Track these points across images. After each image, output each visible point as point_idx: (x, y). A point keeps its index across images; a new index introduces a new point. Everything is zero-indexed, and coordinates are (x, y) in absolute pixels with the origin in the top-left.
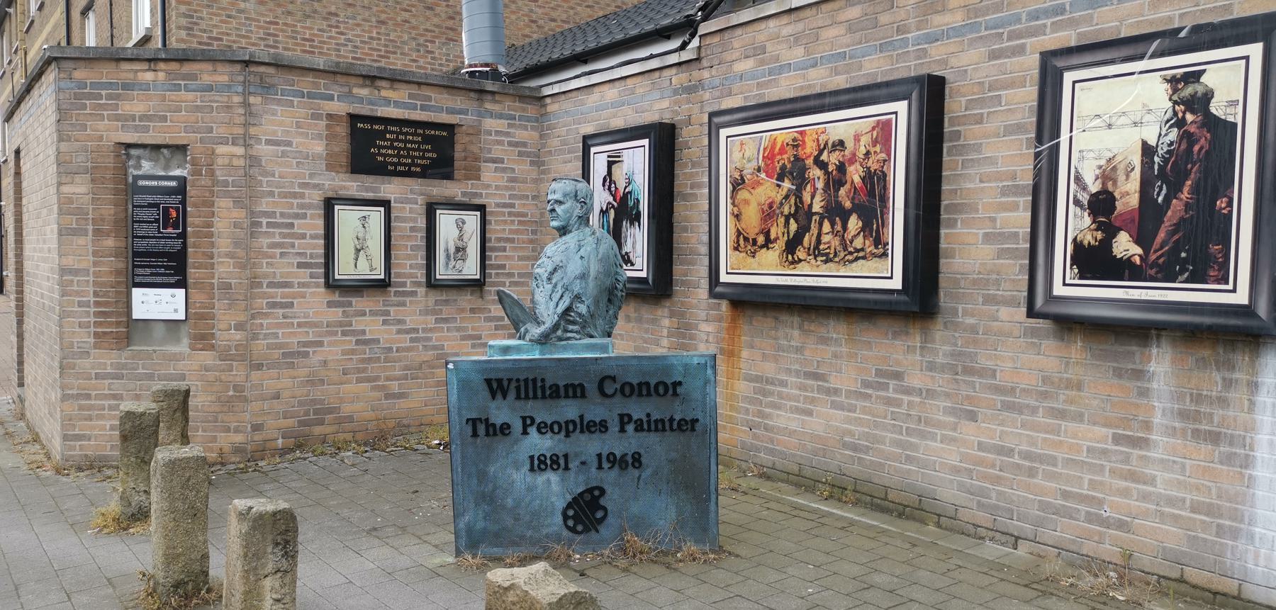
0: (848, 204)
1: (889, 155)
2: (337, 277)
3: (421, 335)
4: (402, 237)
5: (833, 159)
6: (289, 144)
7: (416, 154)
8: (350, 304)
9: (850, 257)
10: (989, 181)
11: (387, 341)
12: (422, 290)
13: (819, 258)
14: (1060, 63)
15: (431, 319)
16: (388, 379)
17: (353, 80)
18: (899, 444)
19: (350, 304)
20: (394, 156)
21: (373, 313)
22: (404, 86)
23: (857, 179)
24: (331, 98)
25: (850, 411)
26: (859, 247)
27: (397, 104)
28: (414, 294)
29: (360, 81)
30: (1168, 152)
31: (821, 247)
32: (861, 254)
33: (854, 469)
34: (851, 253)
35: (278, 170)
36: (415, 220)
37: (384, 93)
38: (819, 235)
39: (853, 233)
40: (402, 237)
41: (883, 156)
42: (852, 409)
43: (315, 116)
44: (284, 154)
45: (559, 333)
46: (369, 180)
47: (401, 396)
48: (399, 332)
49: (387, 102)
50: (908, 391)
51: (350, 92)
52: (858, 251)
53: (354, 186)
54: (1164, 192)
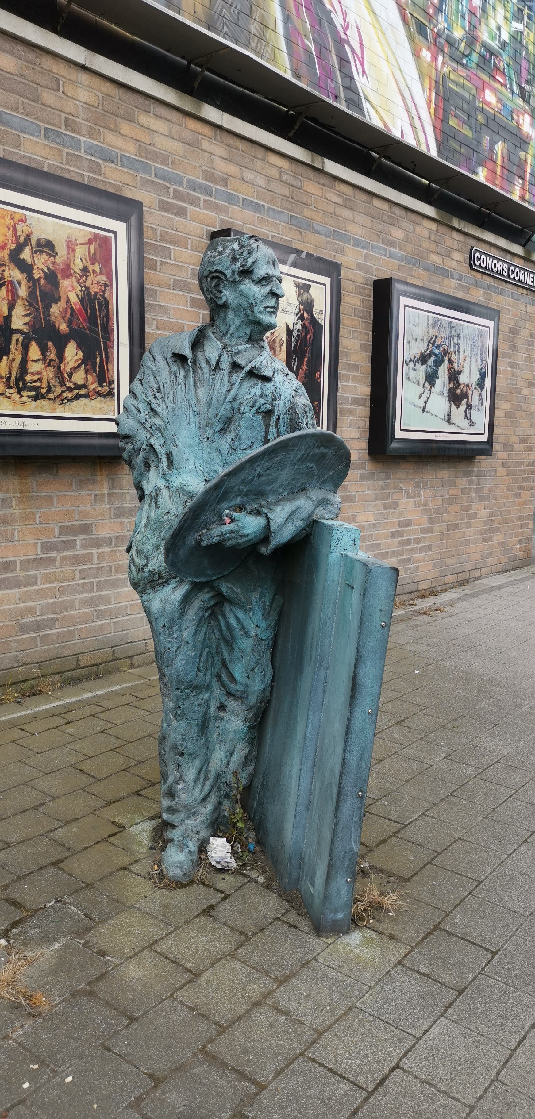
0: (63, 327)
1: (110, 278)
5: (41, 263)
9: (69, 395)
10: (164, 329)
13: (25, 393)
14: (133, 220)
18: (85, 603)
23: (74, 299)
25: (27, 585)
26: (80, 382)
30: (298, 336)
31: (28, 378)
32: (83, 391)
33: (39, 651)
34: (70, 389)
38: (24, 362)
39: (72, 365)
41: (103, 278)
42: (31, 581)
50: (97, 544)
52: (79, 387)
54: (296, 363)
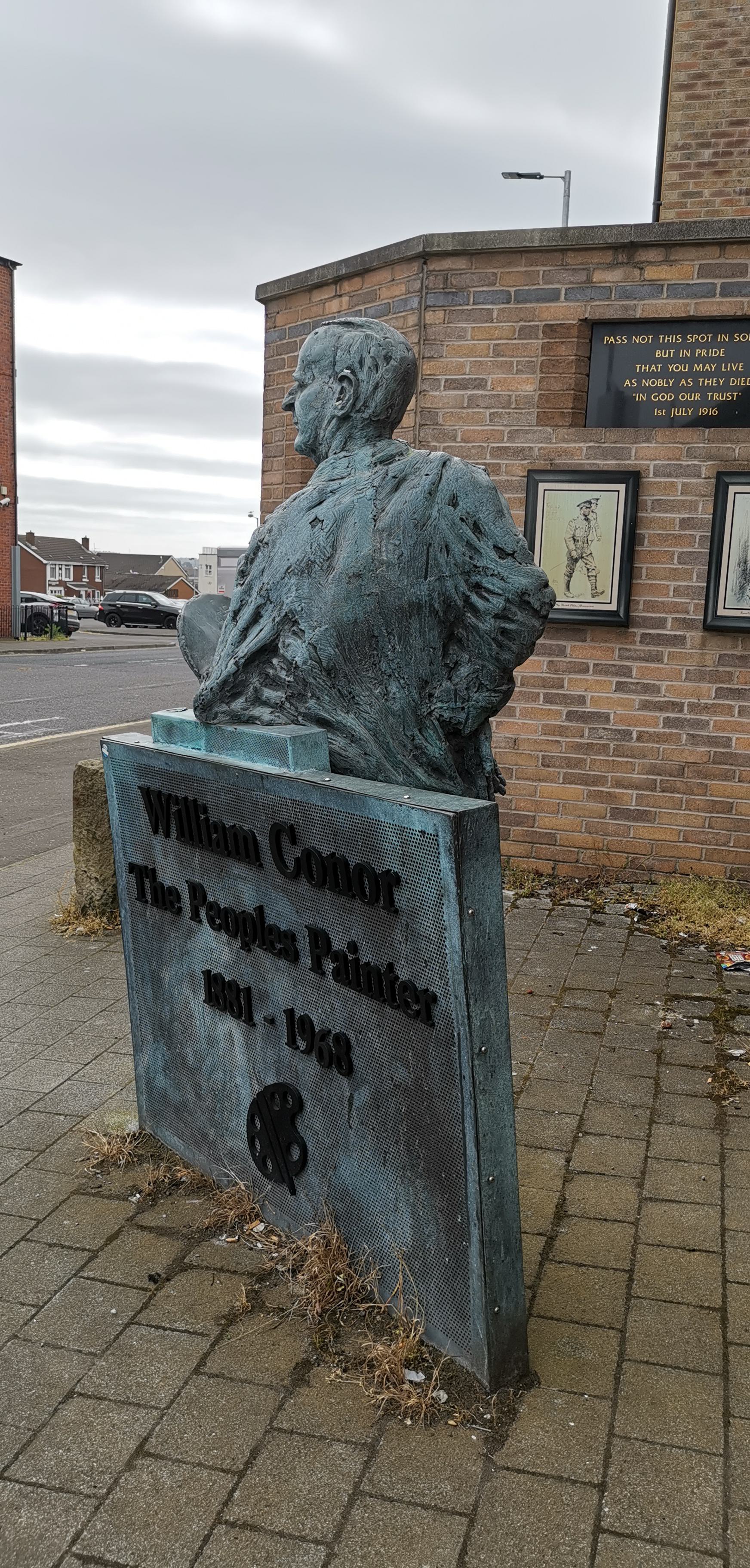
2: (721, 612)
3: (686, 715)
4: (664, 539)
6: (481, 384)
7: (712, 382)
8: (562, 652)
11: (621, 719)
12: (694, 636)
15: (709, 688)
16: (618, 784)
17: (596, 258)
19: (562, 652)
20: (666, 390)
21: (600, 669)
22: (692, 253)
24: (554, 296)
27: (675, 291)
28: (677, 641)
29: (608, 257)
35: (462, 428)
36: (692, 507)
37: (650, 273)
40: (664, 539)
43: (526, 333)
44: (472, 402)
45: (238, 704)
46: (611, 438)
47: (641, 816)
48: (645, 706)
49: (657, 287)
51: (589, 280)
53: (580, 450)
